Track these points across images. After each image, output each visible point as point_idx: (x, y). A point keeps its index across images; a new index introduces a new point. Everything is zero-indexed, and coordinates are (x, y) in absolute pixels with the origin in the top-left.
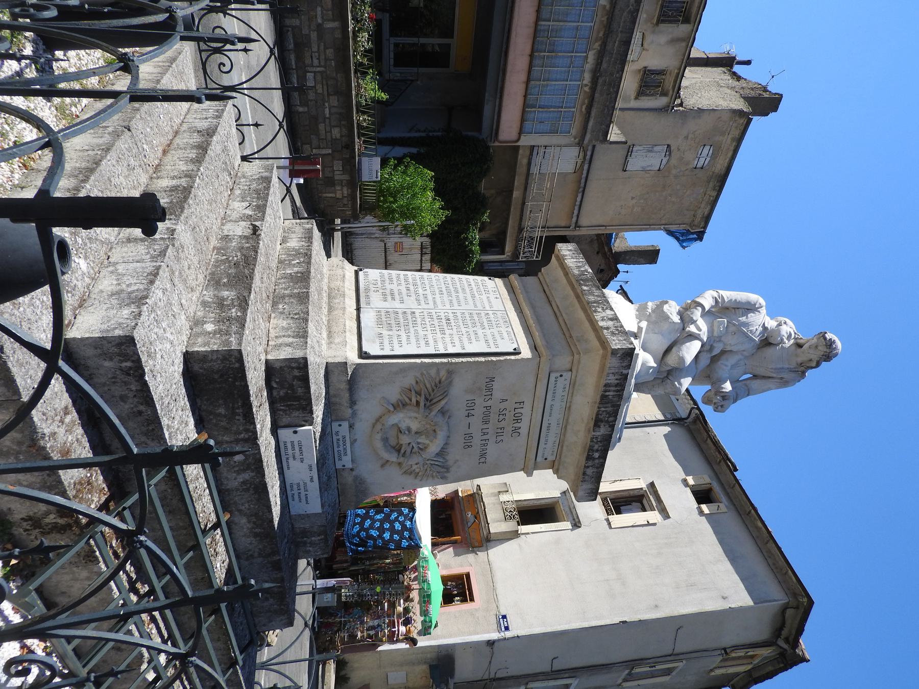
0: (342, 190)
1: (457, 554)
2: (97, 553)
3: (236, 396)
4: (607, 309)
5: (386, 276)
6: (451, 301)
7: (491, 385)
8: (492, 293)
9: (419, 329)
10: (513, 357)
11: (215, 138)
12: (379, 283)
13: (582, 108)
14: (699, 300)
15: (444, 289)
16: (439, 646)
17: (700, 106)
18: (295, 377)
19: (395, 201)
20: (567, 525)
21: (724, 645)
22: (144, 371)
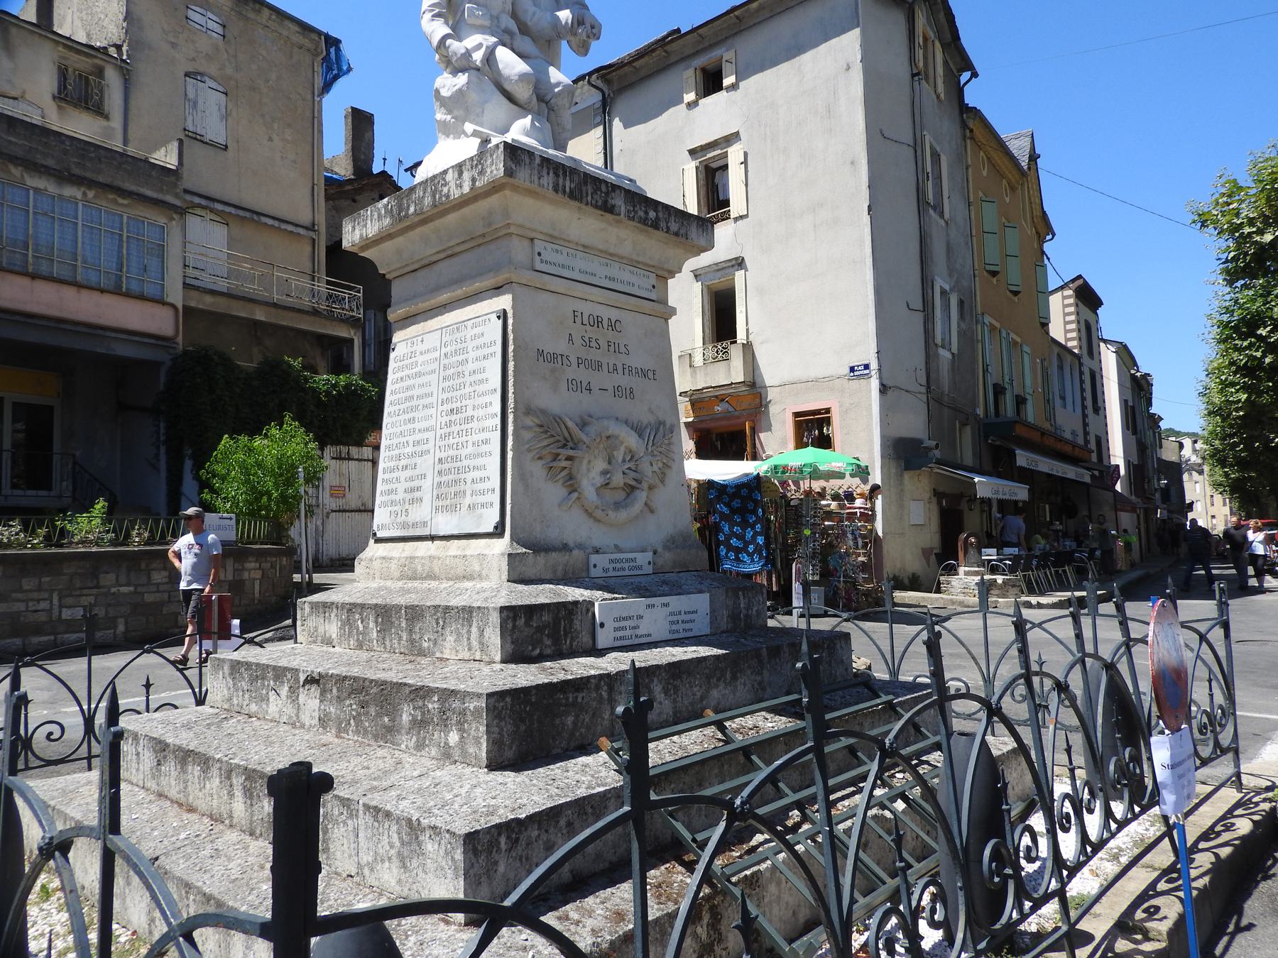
0: (249, 570)
1: (769, 428)
2: (748, 872)
3: (551, 701)
4: (444, 179)
5: (385, 498)
6: (425, 407)
8: (415, 347)
9: (464, 452)
10: (510, 321)
11: (170, 741)
12: (396, 508)
13: (122, 205)
14: (435, 42)
15: (407, 416)
16: (882, 457)
17: (121, 17)
18: (527, 624)
19: (269, 494)
20: (739, 276)
21: (907, 76)
22: (513, 820)
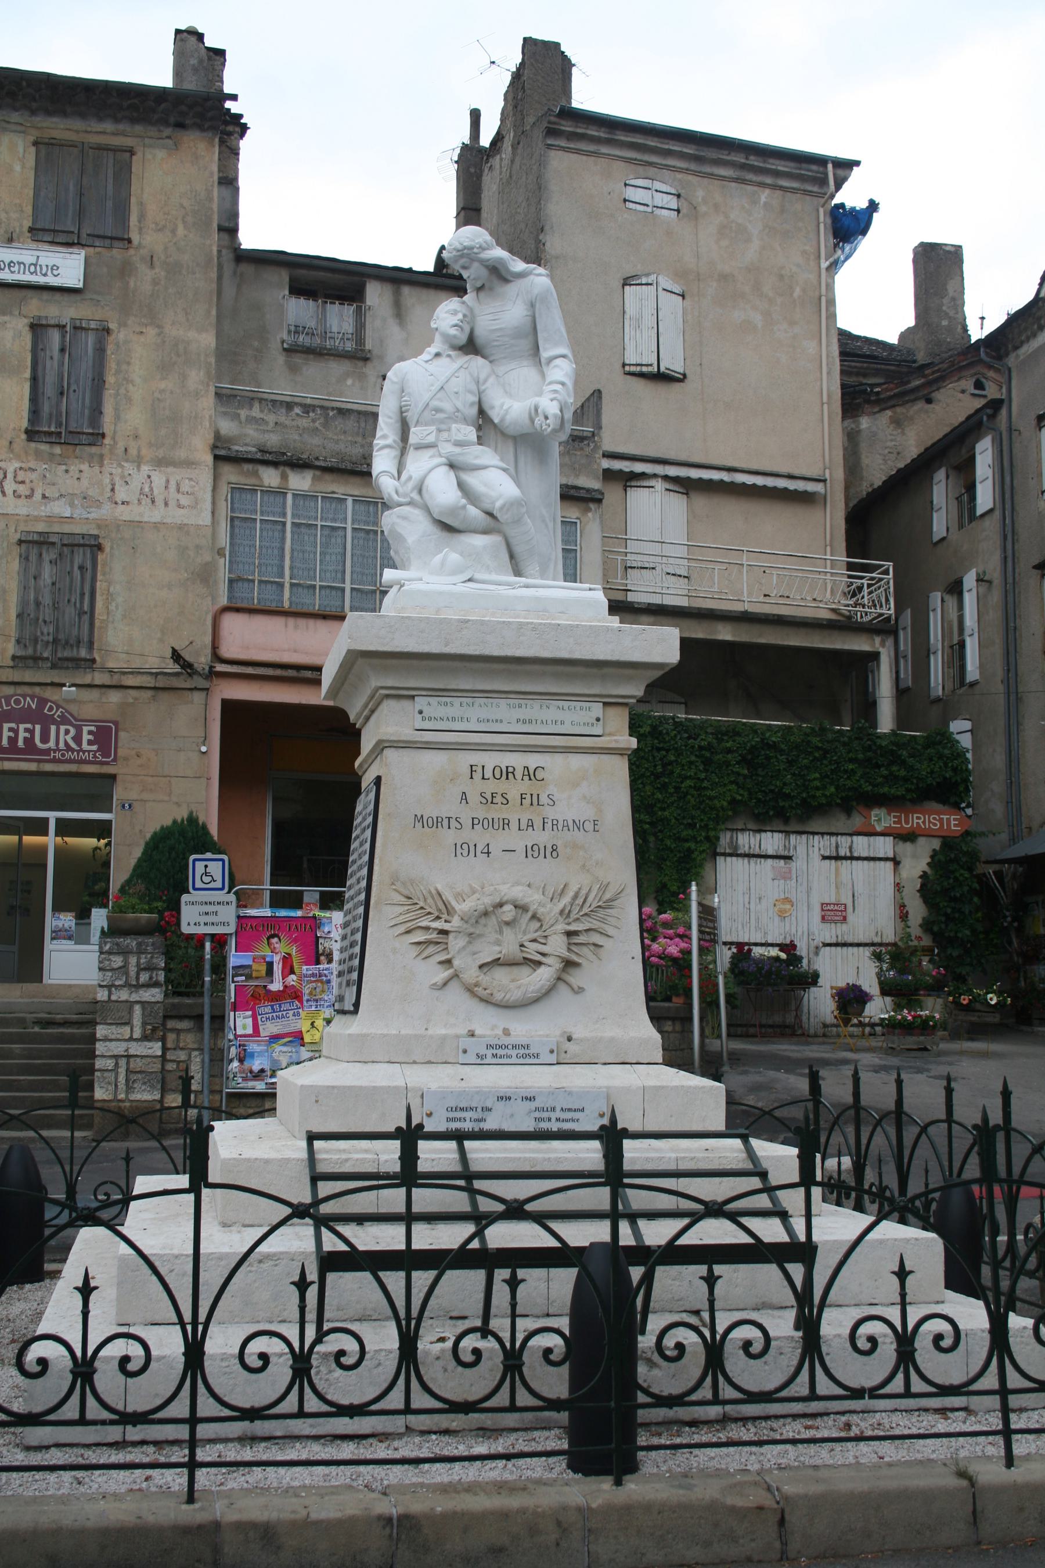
7: (430, 820)
